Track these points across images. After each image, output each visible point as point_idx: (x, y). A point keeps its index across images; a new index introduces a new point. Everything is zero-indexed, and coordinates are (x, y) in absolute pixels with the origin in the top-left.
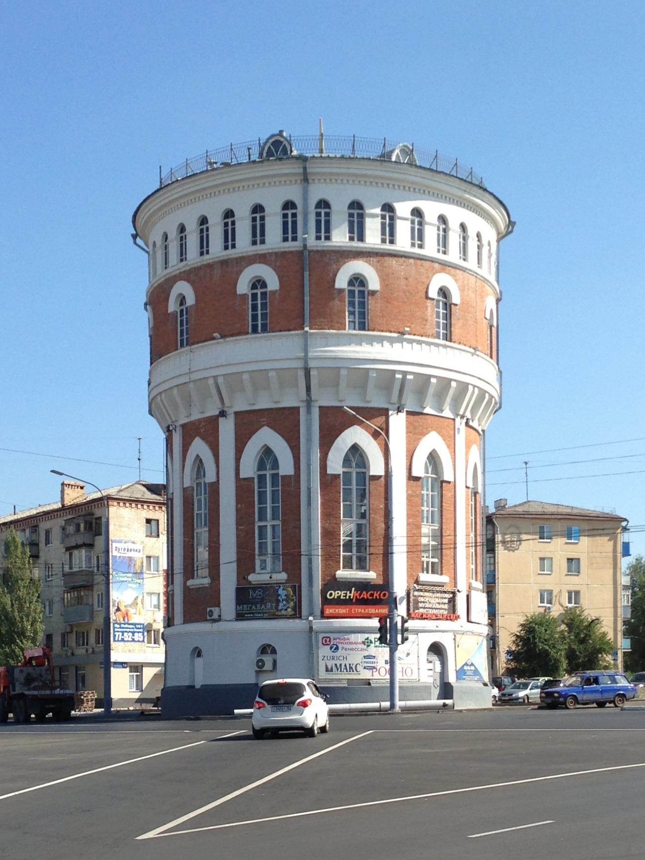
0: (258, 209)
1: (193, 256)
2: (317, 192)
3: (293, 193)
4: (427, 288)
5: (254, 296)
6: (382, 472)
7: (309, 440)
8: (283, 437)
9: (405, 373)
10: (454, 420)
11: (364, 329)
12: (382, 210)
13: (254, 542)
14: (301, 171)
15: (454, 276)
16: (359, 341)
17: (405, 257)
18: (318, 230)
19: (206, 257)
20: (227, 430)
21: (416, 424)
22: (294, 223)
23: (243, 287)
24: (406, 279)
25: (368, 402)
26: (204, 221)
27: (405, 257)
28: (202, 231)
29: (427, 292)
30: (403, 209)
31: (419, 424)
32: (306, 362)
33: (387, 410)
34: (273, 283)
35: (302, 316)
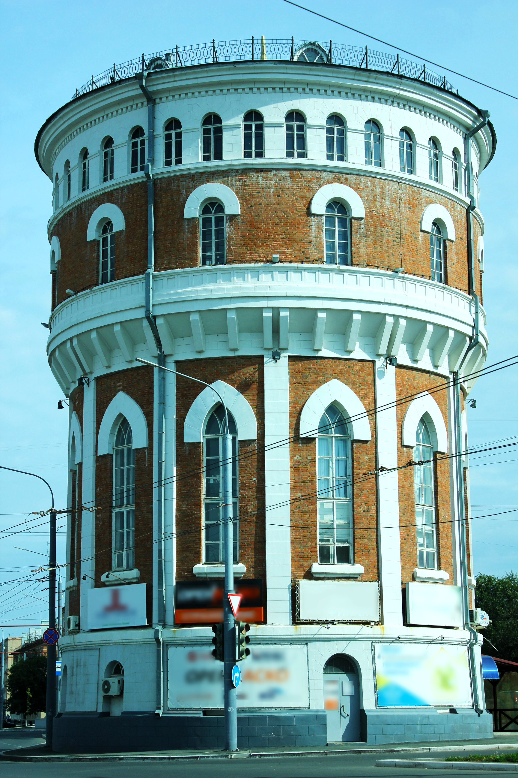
0: (254, 117)
1: (123, 174)
2: (166, 111)
3: (138, 117)
4: (310, 203)
5: (206, 222)
6: (368, 437)
7: (163, 403)
8: (137, 402)
9: (276, 310)
10: (373, 362)
11: (222, 263)
12: (245, 119)
13: (199, 544)
14: (140, 91)
15: (346, 182)
16: (214, 277)
17: (277, 170)
18: (168, 154)
19: (174, 167)
20: (277, 376)
21: (307, 372)
22: (143, 150)
23: (319, 206)
24: (278, 196)
25: (236, 350)
26: (108, 142)
27: (277, 170)
28: (106, 155)
29: (309, 209)
30: (274, 113)
31: (308, 372)
32: (148, 310)
33: (262, 357)
34: (233, 206)
35: (145, 257)
